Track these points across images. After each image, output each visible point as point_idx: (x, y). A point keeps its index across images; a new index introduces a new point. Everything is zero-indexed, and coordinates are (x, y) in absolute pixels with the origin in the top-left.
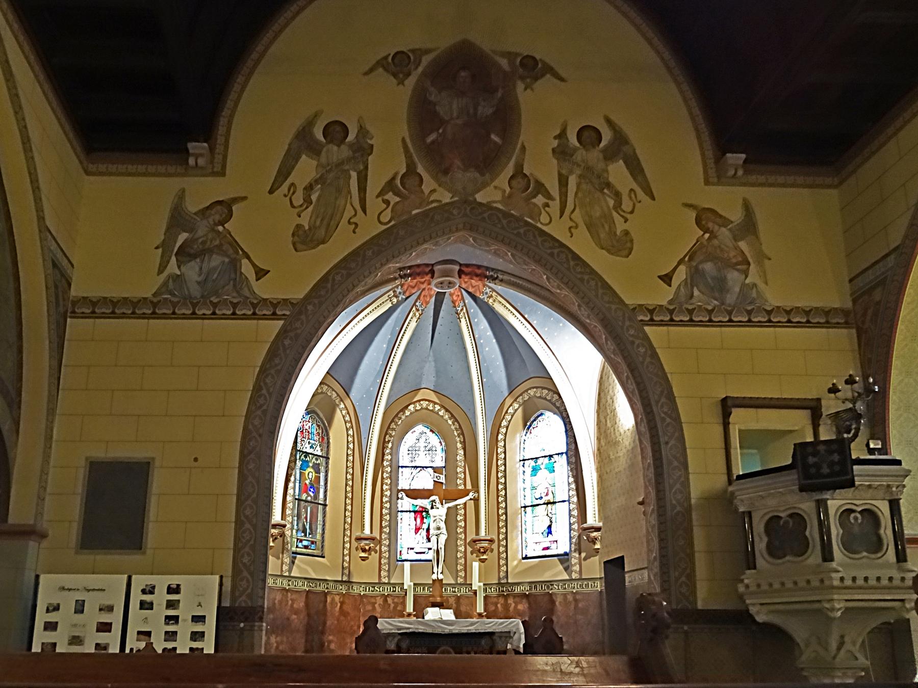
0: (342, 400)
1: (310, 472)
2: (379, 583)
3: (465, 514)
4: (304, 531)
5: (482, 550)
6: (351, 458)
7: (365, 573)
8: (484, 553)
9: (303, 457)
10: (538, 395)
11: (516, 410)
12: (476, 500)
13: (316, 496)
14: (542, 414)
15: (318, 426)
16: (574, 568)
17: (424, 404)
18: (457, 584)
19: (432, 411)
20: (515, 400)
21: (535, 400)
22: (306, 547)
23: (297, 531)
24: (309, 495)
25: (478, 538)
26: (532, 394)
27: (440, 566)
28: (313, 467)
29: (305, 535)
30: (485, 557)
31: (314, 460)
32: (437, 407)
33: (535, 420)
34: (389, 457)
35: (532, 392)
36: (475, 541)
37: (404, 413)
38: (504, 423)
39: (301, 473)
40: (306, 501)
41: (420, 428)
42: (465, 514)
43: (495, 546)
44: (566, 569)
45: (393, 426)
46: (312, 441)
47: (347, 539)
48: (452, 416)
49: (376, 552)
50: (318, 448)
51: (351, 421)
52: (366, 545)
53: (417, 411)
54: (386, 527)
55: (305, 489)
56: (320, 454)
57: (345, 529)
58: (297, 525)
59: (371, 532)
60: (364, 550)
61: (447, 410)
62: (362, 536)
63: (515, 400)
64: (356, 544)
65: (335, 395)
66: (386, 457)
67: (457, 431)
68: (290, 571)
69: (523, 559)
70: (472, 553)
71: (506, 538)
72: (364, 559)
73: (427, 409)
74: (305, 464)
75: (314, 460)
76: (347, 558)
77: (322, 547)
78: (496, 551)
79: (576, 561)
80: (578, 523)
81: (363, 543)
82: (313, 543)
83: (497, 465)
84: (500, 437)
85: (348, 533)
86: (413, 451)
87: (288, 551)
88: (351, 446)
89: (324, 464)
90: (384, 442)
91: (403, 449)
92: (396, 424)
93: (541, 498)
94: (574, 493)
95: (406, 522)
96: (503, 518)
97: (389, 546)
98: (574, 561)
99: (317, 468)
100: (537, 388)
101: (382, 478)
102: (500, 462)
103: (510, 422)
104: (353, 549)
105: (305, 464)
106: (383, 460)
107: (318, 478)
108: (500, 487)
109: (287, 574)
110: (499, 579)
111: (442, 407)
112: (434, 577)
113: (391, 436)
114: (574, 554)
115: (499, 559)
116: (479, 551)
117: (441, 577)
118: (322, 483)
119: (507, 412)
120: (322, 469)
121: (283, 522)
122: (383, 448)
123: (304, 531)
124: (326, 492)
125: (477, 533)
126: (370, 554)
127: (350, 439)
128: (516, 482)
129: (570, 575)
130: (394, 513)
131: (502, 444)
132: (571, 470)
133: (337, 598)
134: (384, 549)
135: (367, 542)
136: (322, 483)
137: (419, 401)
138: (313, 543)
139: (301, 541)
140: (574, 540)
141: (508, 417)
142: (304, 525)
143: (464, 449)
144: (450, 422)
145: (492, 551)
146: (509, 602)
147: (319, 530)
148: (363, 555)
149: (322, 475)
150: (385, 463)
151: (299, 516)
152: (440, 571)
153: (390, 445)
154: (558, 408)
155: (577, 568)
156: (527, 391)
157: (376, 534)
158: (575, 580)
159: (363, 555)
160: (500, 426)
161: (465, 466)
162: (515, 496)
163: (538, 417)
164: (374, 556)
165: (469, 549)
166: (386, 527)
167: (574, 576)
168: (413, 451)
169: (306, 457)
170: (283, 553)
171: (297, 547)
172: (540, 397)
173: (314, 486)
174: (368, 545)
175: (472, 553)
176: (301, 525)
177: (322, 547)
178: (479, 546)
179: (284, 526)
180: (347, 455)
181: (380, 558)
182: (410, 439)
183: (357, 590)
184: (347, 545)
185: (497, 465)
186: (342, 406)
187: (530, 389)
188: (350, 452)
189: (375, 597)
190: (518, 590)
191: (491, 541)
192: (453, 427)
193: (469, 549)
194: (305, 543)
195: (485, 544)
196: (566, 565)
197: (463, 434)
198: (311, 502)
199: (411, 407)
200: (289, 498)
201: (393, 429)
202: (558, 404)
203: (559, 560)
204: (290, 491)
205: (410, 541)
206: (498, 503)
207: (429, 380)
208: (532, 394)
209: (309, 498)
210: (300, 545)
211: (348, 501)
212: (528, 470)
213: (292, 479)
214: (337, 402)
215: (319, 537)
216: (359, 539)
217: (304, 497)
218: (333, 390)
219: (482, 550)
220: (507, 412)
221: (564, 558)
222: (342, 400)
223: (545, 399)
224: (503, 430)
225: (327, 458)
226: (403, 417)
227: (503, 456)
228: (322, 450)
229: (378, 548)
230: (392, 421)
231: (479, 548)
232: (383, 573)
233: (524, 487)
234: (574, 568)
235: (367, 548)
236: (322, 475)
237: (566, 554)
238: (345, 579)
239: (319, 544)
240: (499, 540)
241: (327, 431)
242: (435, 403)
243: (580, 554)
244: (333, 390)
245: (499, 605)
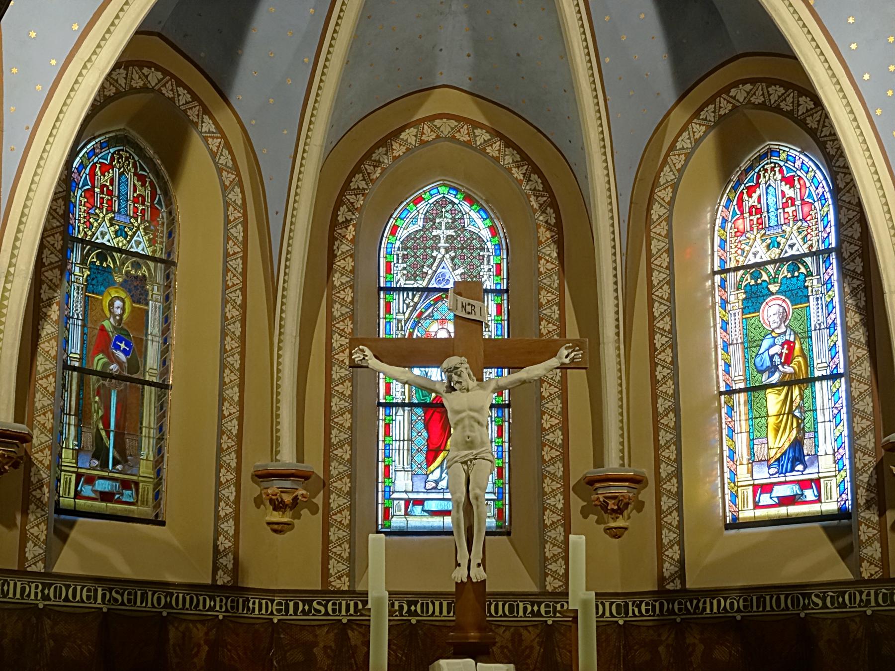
0: (206, 111)
1: (116, 303)
2: (324, 592)
3: (565, 411)
4: (100, 453)
5: (612, 505)
6: (237, 264)
7: (283, 562)
8: (619, 511)
9: (93, 258)
10: (757, 99)
11: (698, 142)
12: (592, 366)
13: (136, 361)
14: (770, 153)
15: (142, 179)
16: (868, 551)
17: (446, 127)
18: (545, 593)
19: (467, 144)
20: (696, 115)
21: (751, 113)
22: (106, 496)
23: (78, 452)
24: (113, 359)
25: (600, 472)
26: (741, 97)
27: (477, 547)
28: (123, 285)
29: (104, 465)
30: (620, 523)
31: (128, 267)
32: (482, 136)
33: (751, 168)
34: (349, 263)
35: (740, 94)
36: (591, 482)
37: (389, 149)
38: (667, 175)
39: (87, 300)
40: (104, 375)
41: (435, 192)
42: (565, 411)
43: (647, 495)
44: (846, 553)
45: (358, 182)
46: (122, 219)
47: (227, 476)
48: (524, 158)
49: (314, 510)
50: (141, 236)
51: (236, 168)
52: (285, 491)
53: (423, 143)
54: (341, 445)
55: (101, 342)
56: (149, 252)
57: (220, 450)
58: (78, 437)
59: (300, 458)
60: (278, 506)
61: (508, 143)
62: (272, 467)
63: (696, 115)
64: (256, 490)
65: (184, 97)
66: (340, 263)
67: (539, 185)
68: (50, 558)
69: (728, 527)
70: (585, 513)
71: (678, 474)
72: (278, 529)
73: (453, 139)
74: (99, 279)
75: (128, 267)
76: (228, 527)
77: (157, 496)
78: (650, 509)
79: (872, 532)
80: (875, 431)
81: (275, 487)
82: (126, 485)
83: (652, 318)
84: (657, 211)
85: (231, 459)
86: (418, 249)
87: (40, 504)
88: (237, 232)
89: (160, 277)
90: (334, 223)
91: (391, 246)
92: (367, 178)
93: (773, 369)
94: (863, 352)
95: (402, 429)
96: (671, 419)
97: (351, 493)
98: (865, 532)
99: (137, 288)
100: (753, 81)
101: (330, 317)
102: (657, 277)
103: (681, 171)
104: (247, 504)
105: (99, 279)
106: (330, 270)
107: (141, 318)
108: (659, 340)
109: (40, 567)
110: (661, 579)
111: (497, 134)
112: (461, 574)
113: (352, 209)
114: (866, 514)
115: (659, 528)
116: (604, 507)
117: (478, 574)
118: (154, 327)
119: (672, 147)
120: (155, 291)
121: (22, 428)
122: (332, 239)
123: (100, 453)
124: (165, 351)
125: (599, 460)
126: (298, 516)
127: (234, 214)
128: (704, 328)
129: (855, 568)
130: (367, 408)
131: (662, 229)
132: (854, 292)
133: (199, 633)
134: (336, 501)
135: (287, 484)
136: (154, 327)
137: (432, 118)
138: (126, 485)
139: (90, 480)
140: (865, 478)
141: (678, 160)
142: (98, 439)
143: (560, 244)
144: (518, 174)
145: (640, 506)
146: (690, 640)
147: (147, 451)
148: (276, 517)
149: (154, 309)
150: (337, 279)
151: (82, 414)
152: (476, 559)
153: (350, 232)
154: (812, 133)
155: (874, 551)
156: (726, 90)
157: (314, 464)
158: (870, 582)
159: (276, 517)
160: (655, 184)
161: (561, 285)
162: (704, 361)
163: (761, 158)
164: (309, 524)
165: (577, 503)
166: (341, 445)
167: (868, 571)
168: (418, 249)
169: (102, 257)
170: (25, 512)
171: (77, 495)
172: (763, 106)
173: (131, 336)
174: (290, 493)
175: (585, 513)
176: (88, 438)
177: (157, 496)
178: (602, 493)
179: (25, 439)
180: (226, 254)
181: (326, 526)
182: (410, 221)
183: (258, 609)
184: (229, 493)
185: (652, 318)
186: (208, 126)
187: (735, 85)
188: (233, 248)
189: (311, 628)
190: (712, 608)
191: (637, 481)
192: (526, 187)
193: (577, 503)
194: (103, 485)
195: (621, 490)
196: (843, 542)
197: (554, 204)
198: (119, 378)
199: (410, 135)
200: (43, 364)
201: (359, 191)
202: (811, 123)
203: (825, 528)
204: (48, 346)
205: (414, 487)
206: (654, 382)
207: (454, 63)
208: (741, 97)
209: (114, 367)
210: (87, 490)
211: (231, 377)
212: (736, 298)
213: (54, 312)
214: (193, 114)
215: (145, 469)
216: (263, 476)
217: (99, 362)
218: (179, 83)
219: (612, 505)
220: (672, 147)
221: (838, 525)
222: (206, 111)
223: (778, 110)
224: (664, 194)
225: (169, 263)
226: (386, 160)
227: (665, 260)
228: (152, 242)
229: (319, 500)
230: (357, 170)
231: (607, 499)
232: (335, 567)
233: (727, 341)
234: (868, 551)
235: (287, 498)
236: (154, 309)
237: (842, 514)
238: (223, 579)
239: (146, 488)
240: (658, 480)
241: (166, 192)
242: (476, 125)
243: (882, 514)
244: (179, 83)
245: (661, 649)
